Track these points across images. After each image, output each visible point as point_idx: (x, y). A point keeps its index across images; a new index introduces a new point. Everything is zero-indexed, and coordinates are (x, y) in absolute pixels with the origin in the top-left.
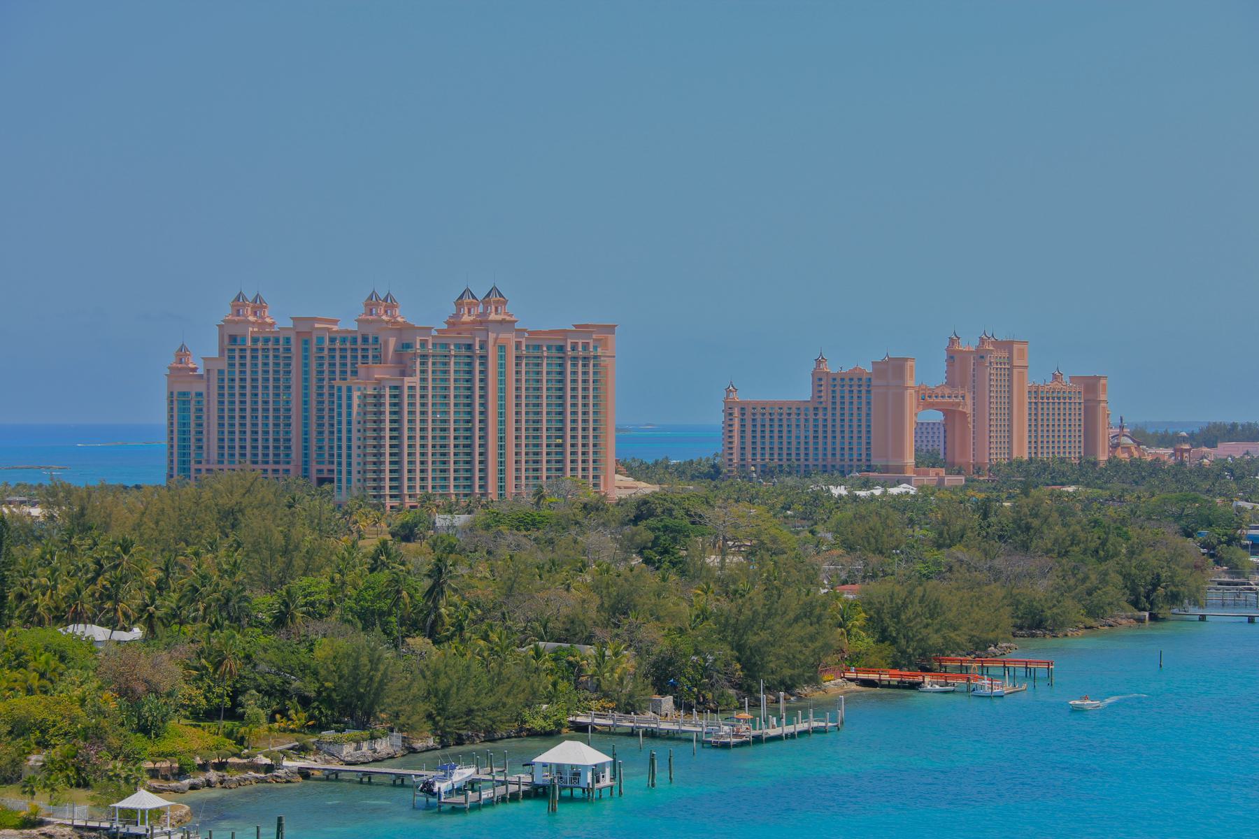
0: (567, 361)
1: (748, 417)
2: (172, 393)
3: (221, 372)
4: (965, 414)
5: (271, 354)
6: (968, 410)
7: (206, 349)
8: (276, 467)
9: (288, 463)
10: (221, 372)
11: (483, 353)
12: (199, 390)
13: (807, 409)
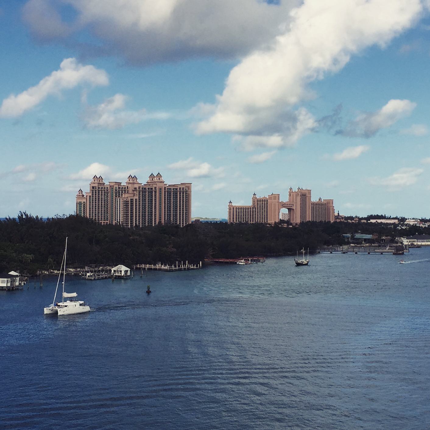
0: (372, 215)
1: (235, 210)
2: (77, 202)
3: (90, 196)
4: (293, 209)
5: (103, 191)
6: (295, 208)
7: (87, 190)
8: (104, 222)
9: (107, 220)
10: (90, 196)
11: (128, 190)
12: (84, 201)
13: (250, 208)
